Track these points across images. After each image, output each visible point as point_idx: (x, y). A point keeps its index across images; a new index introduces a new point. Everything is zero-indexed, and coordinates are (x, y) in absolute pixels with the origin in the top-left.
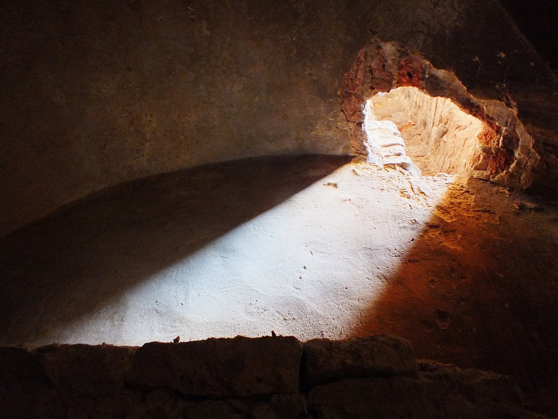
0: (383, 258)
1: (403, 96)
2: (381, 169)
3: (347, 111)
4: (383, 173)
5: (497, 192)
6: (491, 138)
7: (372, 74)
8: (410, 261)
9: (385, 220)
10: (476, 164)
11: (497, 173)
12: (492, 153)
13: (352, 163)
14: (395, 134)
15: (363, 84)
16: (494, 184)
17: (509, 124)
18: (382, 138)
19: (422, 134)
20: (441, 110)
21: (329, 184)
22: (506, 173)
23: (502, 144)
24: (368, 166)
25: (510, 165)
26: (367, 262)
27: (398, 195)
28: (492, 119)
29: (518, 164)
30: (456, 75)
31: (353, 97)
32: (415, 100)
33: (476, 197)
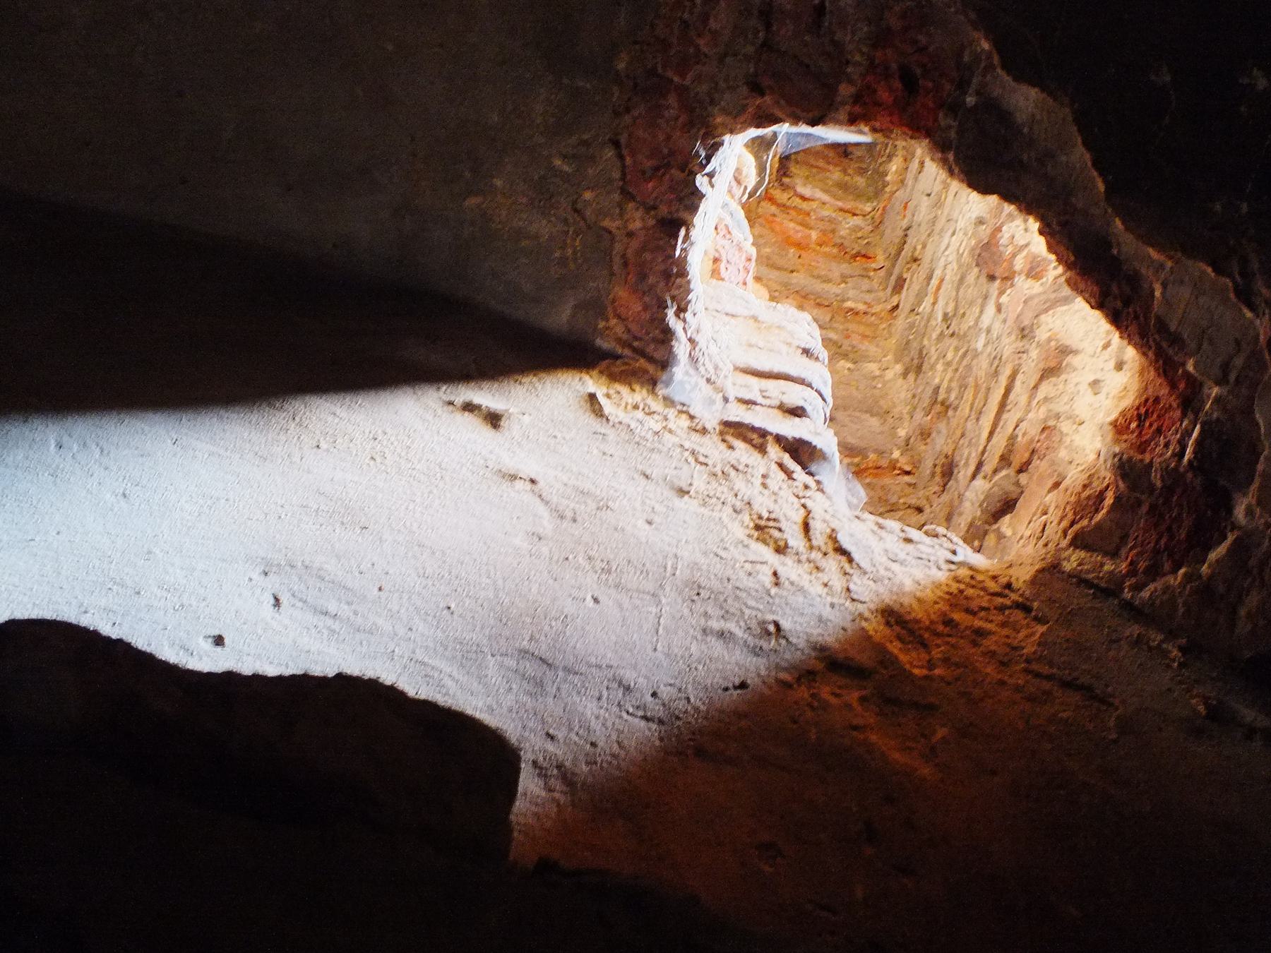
0: (590, 709)
1: (899, 368)
2: (704, 431)
3: (633, 154)
4: (713, 449)
5: (1138, 641)
6: (1159, 431)
7: (768, 26)
8: (700, 752)
9: (650, 586)
10: (1085, 522)
11: (1154, 572)
12: (1152, 488)
13: (595, 373)
14: (806, 352)
15: (721, 59)
16: (1133, 611)
17: (1232, 377)
18: (750, 345)
19: (927, 510)
20: (1019, 415)
21: (469, 407)
22: (1188, 578)
23: (1194, 452)
24: (656, 405)
25: (1208, 548)
26: (509, 700)
27: (739, 529)
28: (1176, 340)
29: (1240, 549)
30: (1076, 121)
31: (672, 100)
32: (937, 381)
33: (1049, 629)
